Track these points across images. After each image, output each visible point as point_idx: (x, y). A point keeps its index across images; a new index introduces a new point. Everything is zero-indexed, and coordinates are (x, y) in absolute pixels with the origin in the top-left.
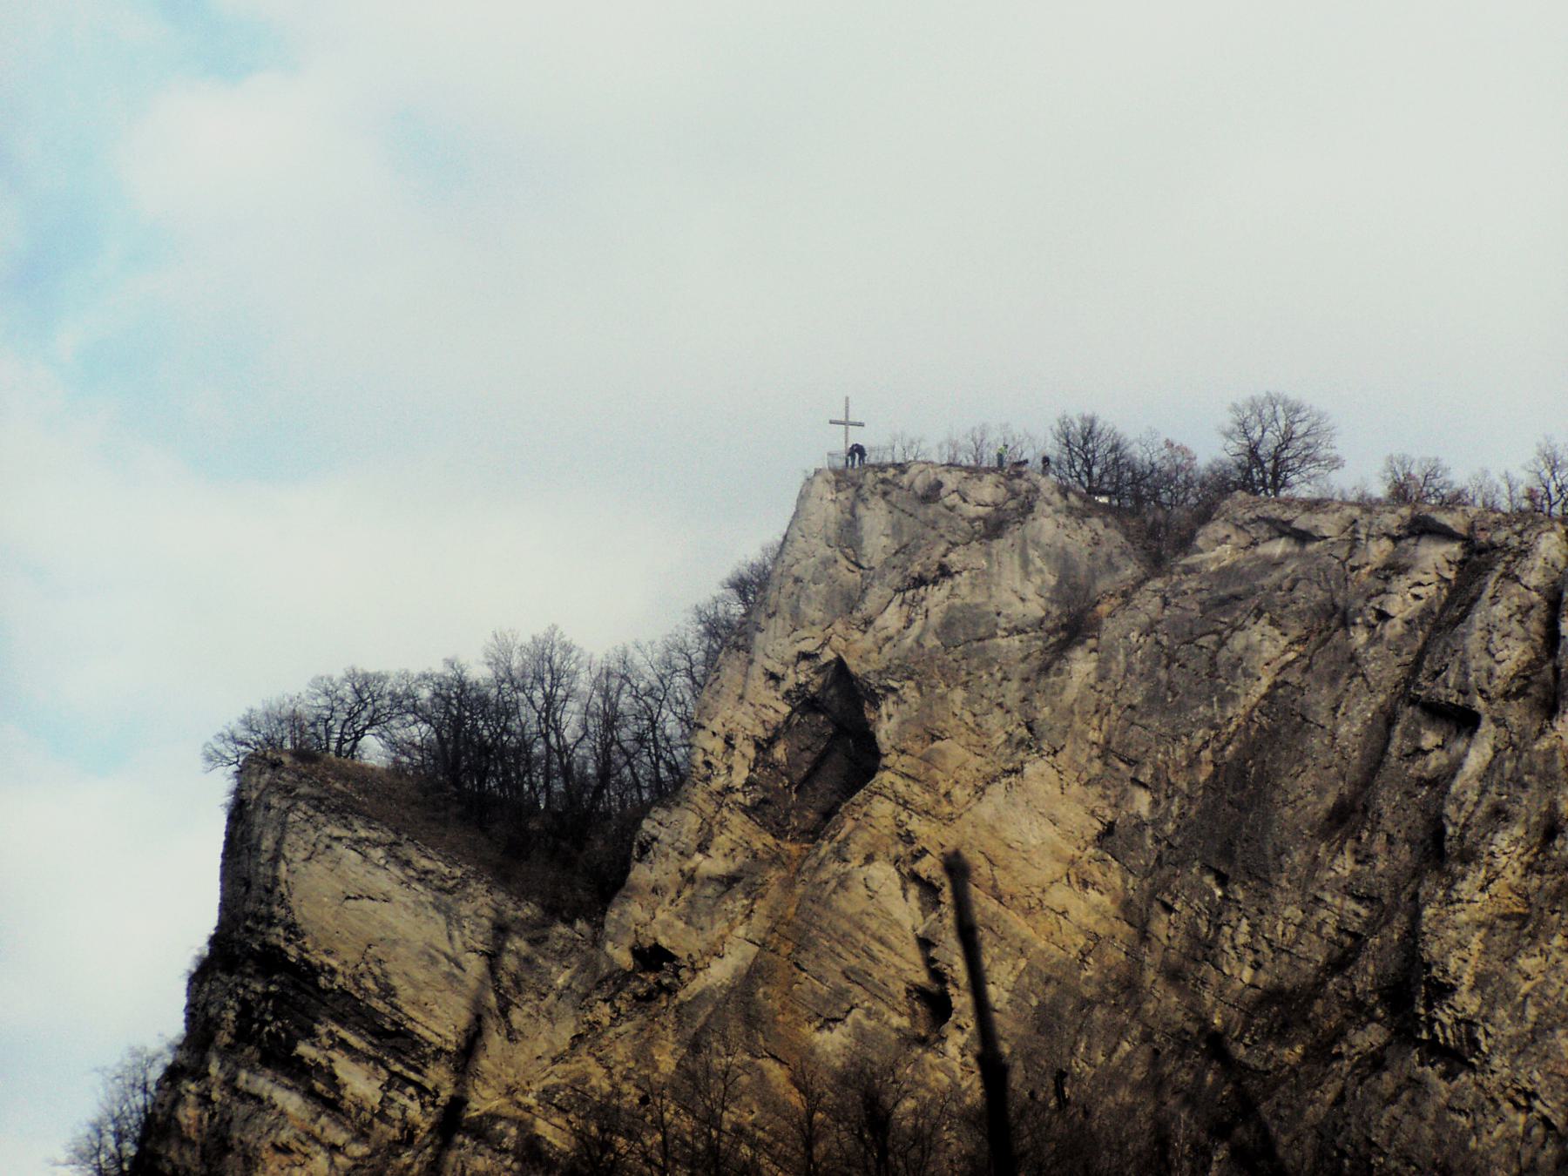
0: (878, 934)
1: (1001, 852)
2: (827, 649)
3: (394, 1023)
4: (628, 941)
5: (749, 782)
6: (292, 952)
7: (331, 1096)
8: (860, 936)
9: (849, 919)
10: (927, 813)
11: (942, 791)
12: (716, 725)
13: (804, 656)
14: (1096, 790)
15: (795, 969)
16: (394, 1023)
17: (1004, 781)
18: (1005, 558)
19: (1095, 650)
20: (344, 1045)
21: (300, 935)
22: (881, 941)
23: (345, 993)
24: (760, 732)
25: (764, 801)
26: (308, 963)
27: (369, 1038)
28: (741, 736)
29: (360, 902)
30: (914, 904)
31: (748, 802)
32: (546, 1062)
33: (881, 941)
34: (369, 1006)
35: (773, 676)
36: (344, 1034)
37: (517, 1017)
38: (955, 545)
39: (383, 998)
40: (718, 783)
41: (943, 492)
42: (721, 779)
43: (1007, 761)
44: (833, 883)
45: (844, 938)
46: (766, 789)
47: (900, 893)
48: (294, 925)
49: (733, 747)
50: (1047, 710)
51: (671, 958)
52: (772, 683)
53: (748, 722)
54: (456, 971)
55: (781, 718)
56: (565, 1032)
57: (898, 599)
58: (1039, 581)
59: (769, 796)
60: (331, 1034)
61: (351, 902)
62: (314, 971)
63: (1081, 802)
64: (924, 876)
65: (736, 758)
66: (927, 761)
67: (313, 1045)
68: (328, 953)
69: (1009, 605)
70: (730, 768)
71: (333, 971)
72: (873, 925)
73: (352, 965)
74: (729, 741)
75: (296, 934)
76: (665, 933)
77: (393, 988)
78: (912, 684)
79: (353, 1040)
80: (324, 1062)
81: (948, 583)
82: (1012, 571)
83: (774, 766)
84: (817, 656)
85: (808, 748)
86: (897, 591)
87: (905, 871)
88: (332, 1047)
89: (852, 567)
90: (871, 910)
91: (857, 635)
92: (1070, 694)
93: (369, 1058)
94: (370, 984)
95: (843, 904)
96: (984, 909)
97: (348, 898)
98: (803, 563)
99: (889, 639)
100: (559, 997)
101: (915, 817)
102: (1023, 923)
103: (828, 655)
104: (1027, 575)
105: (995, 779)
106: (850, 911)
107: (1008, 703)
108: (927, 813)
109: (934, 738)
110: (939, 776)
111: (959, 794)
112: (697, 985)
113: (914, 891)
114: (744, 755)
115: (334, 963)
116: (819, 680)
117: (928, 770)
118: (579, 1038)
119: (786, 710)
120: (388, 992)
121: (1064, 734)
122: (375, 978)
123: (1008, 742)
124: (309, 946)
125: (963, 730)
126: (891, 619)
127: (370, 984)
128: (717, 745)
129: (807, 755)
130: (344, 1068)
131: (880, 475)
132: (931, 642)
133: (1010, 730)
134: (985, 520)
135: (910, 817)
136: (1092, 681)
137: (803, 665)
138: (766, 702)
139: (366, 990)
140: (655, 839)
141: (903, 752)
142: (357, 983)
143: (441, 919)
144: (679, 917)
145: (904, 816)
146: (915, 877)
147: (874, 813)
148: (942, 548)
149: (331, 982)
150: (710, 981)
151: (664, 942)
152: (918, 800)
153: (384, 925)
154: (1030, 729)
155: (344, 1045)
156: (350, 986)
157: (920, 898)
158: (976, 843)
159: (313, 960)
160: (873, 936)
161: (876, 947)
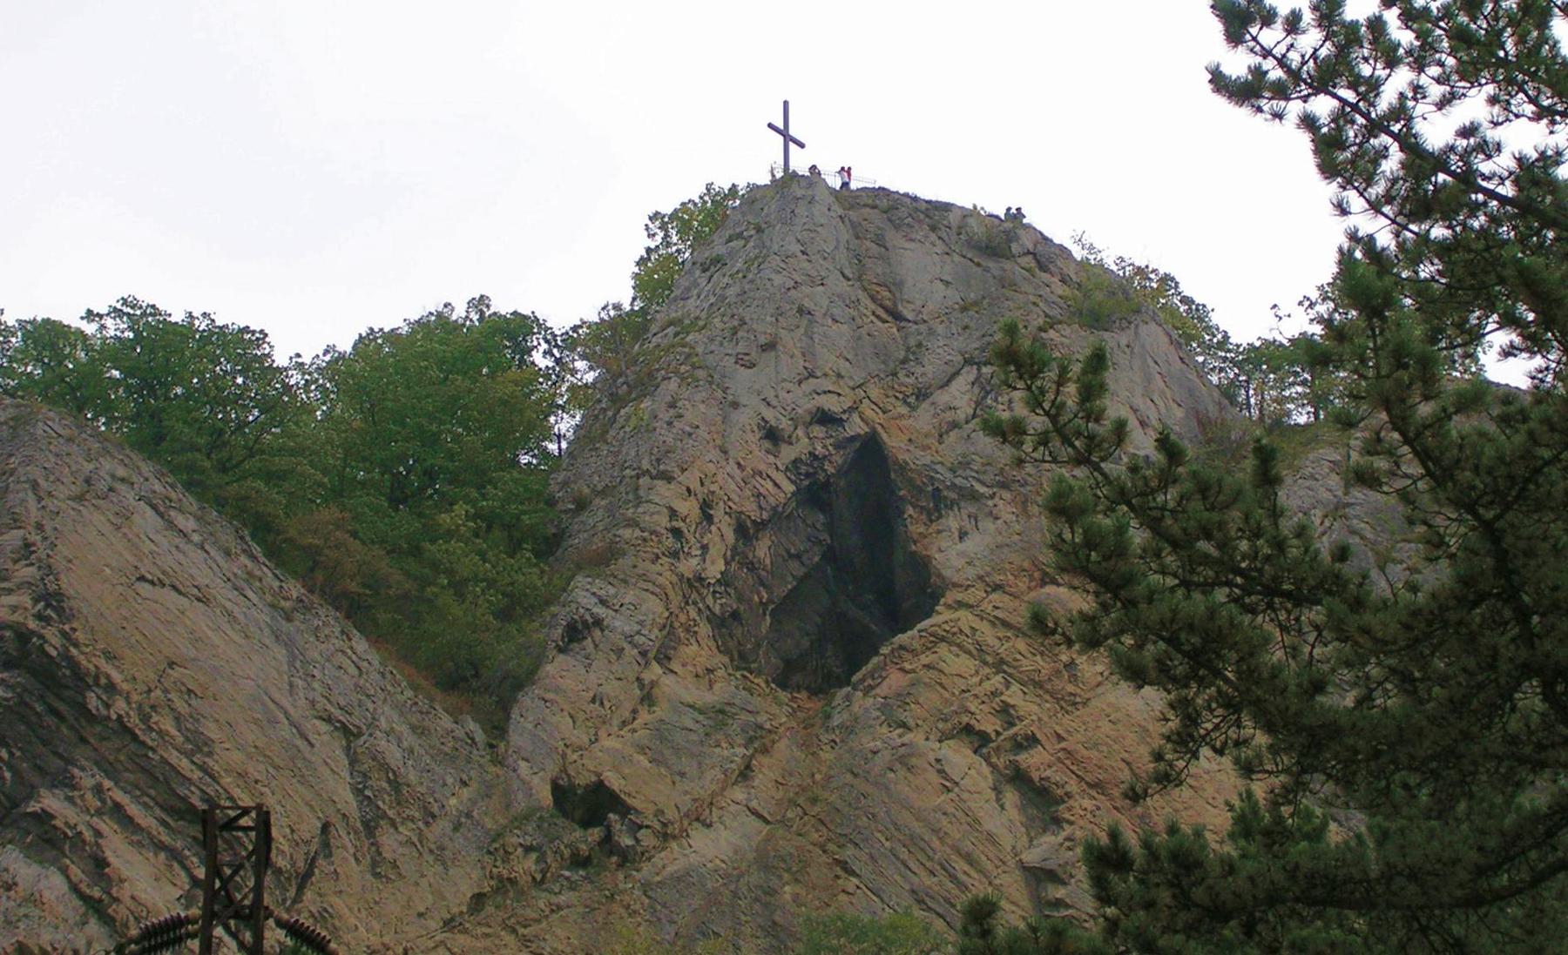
2: (856, 418)
3: (207, 799)
4: (552, 769)
5: (725, 580)
6: (52, 635)
7: (96, 893)
10: (1039, 685)
12: (691, 479)
13: (825, 418)
15: (839, 871)
16: (207, 799)
20: (127, 822)
21: (65, 614)
22: (969, 859)
23: (124, 729)
24: (750, 508)
26: (73, 664)
27: (158, 811)
29: (159, 593)
30: (1013, 813)
32: (433, 924)
33: (969, 859)
34: (164, 761)
35: (772, 436)
36: (119, 796)
37: (389, 841)
39: (189, 755)
40: (689, 566)
42: (694, 561)
45: (913, 842)
46: (740, 599)
48: (59, 595)
51: (624, 810)
52: (767, 444)
54: (300, 742)
56: (465, 881)
57: (969, 374)
60: (98, 790)
61: (145, 588)
62: (81, 679)
65: (712, 538)
67: (70, 800)
68: (110, 657)
70: (705, 548)
71: (111, 687)
73: (142, 687)
74: (706, 506)
75: (60, 611)
76: (616, 768)
77: (208, 742)
79: (133, 810)
80: (88, 835)
83: (752, 567)
85: (798, 557)
86: (968, 362)
87: (1001, 762)
88: (99, 813)
93: (161, 847)
94: (168, 725)
97: (142, 578)
99: (954, 425)
100: (457, 827)
101: (1015, 687)
103: (856, 427)
108: (1039, 685)
112: (672, 860)
113: (1011, 796)
115: (117, 677)
116: (838, 459)
118: (478, 900)
120: (199, 745)
122: (178, 719)
124: (80, 636)
127: (168, 725)
128: (689, 508)
130: (119, 851)
135: (1008, 685)
137: (818, 431)
138: (762, 467)
139: (161, 733)
140: (598, 622)
141: (997, 587)
142: (145, 719)
143: (281, 653)
144: (642, 749)
146: (1019, 777)
149: (108, 706)
150: (694, 859)
151: (614, 781)
152: (1026, 665)
153: (196, 640)
155: (127, 822)
156: (134, 720)
157: (1022, 809)
159: (82, 660)
161: (960, 865)
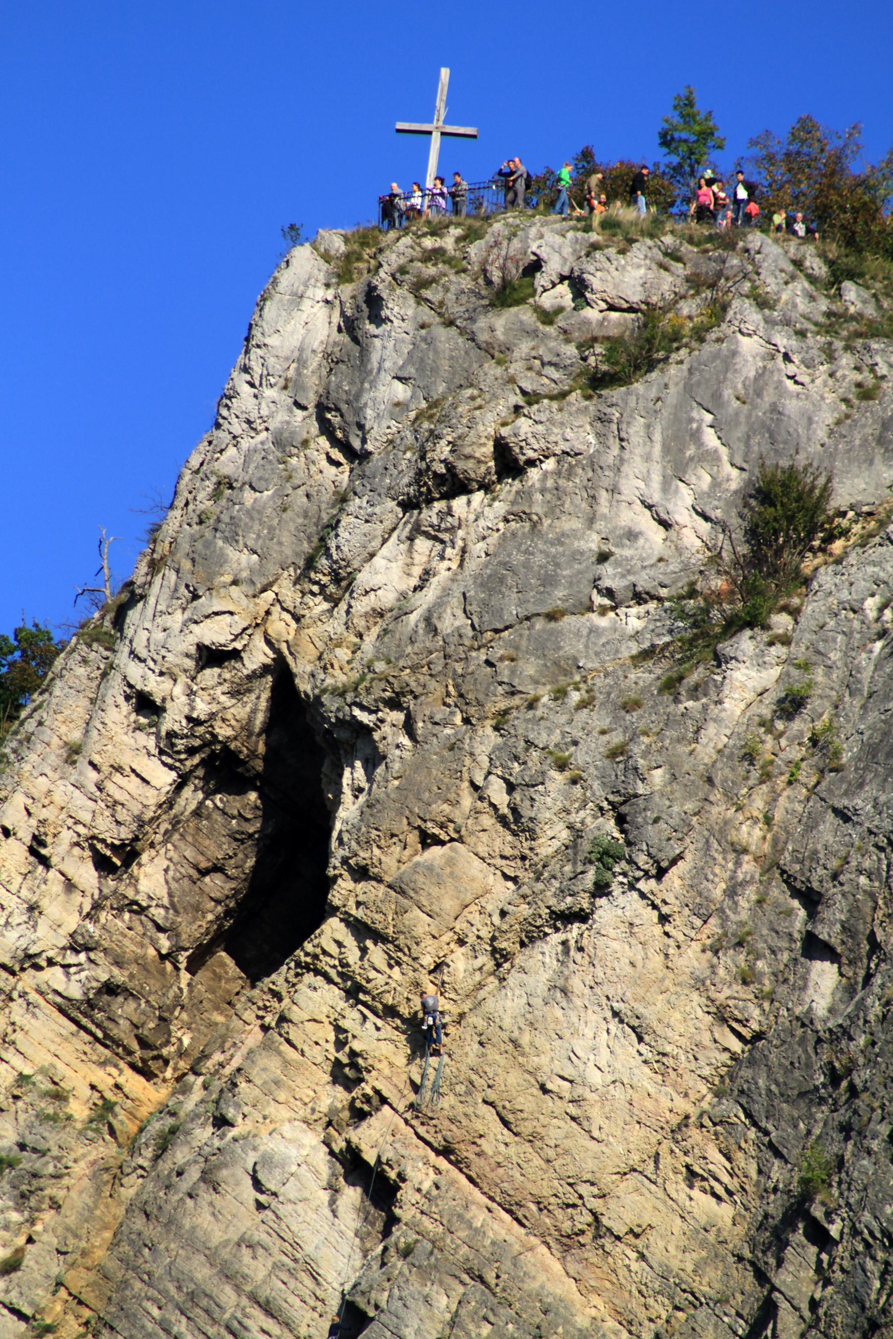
0: (264, 1293)
1: (528, 1101)
8: (228, 1296)
9: (211, 1257)
11: (428, 961)
13: (211, 657)
14: (731, 961)
17: (555, 938)
18: (636, 430)
19: (786, 641)
25: (110, 989)
28: (67, 836)
31: (75, 992)
38: (532, 398)
41: (541, 280)
43: (562, 893)
44: (194, 1174)
47: (325, 1196)
49: (45, 862)
50: (658, 776)
53: (83, 808)
55: (152, 798)
58: (706, 481)
59: (120, 976)
63: (699, 984)
64: (370, 1157)
66: (402, 892)
69: (632, 535)
72: (257, 1269)
78: (398, 717)
81: (509, 488)
82: (648, 458)
84: (236, 655)
85: (217, 869)
89: (337, 455)
90: (261, 1236)
91: (320, 606)
92: (715, 738)
95: (205, 1220)
96: (478, 1232)
98: (245, 444)
102: (557, 1267)
104: (678, 471)
105: (530, 937)
106: (217, 1236)
107: (580, 757)
109: (427, 840)
110: (418, 921)
111: (461, 964)
114: (70, 885)
117: (401, 912)
119: (164, 778)
121: (684, 829)
123: (572, 846)
125: (487, 821)
126: (386, 574)
129: (215, 884)
131: (429, 243)
132: (452, 621)
133: (576, 818)
134: (614, 344)
136: (766, 712)
145: (351, 1020)
147: (296, 1014)
148: (503, 407)
154: (621, 820)
157: (361, 1210)
158: (479, 1082)
160: (253, 1298)
